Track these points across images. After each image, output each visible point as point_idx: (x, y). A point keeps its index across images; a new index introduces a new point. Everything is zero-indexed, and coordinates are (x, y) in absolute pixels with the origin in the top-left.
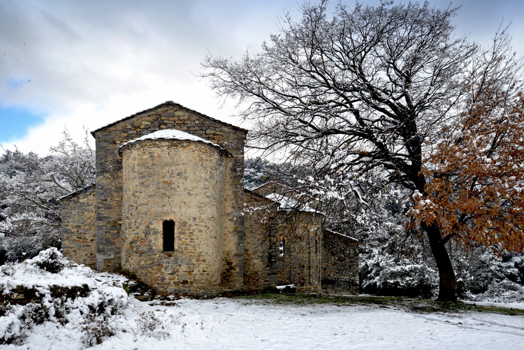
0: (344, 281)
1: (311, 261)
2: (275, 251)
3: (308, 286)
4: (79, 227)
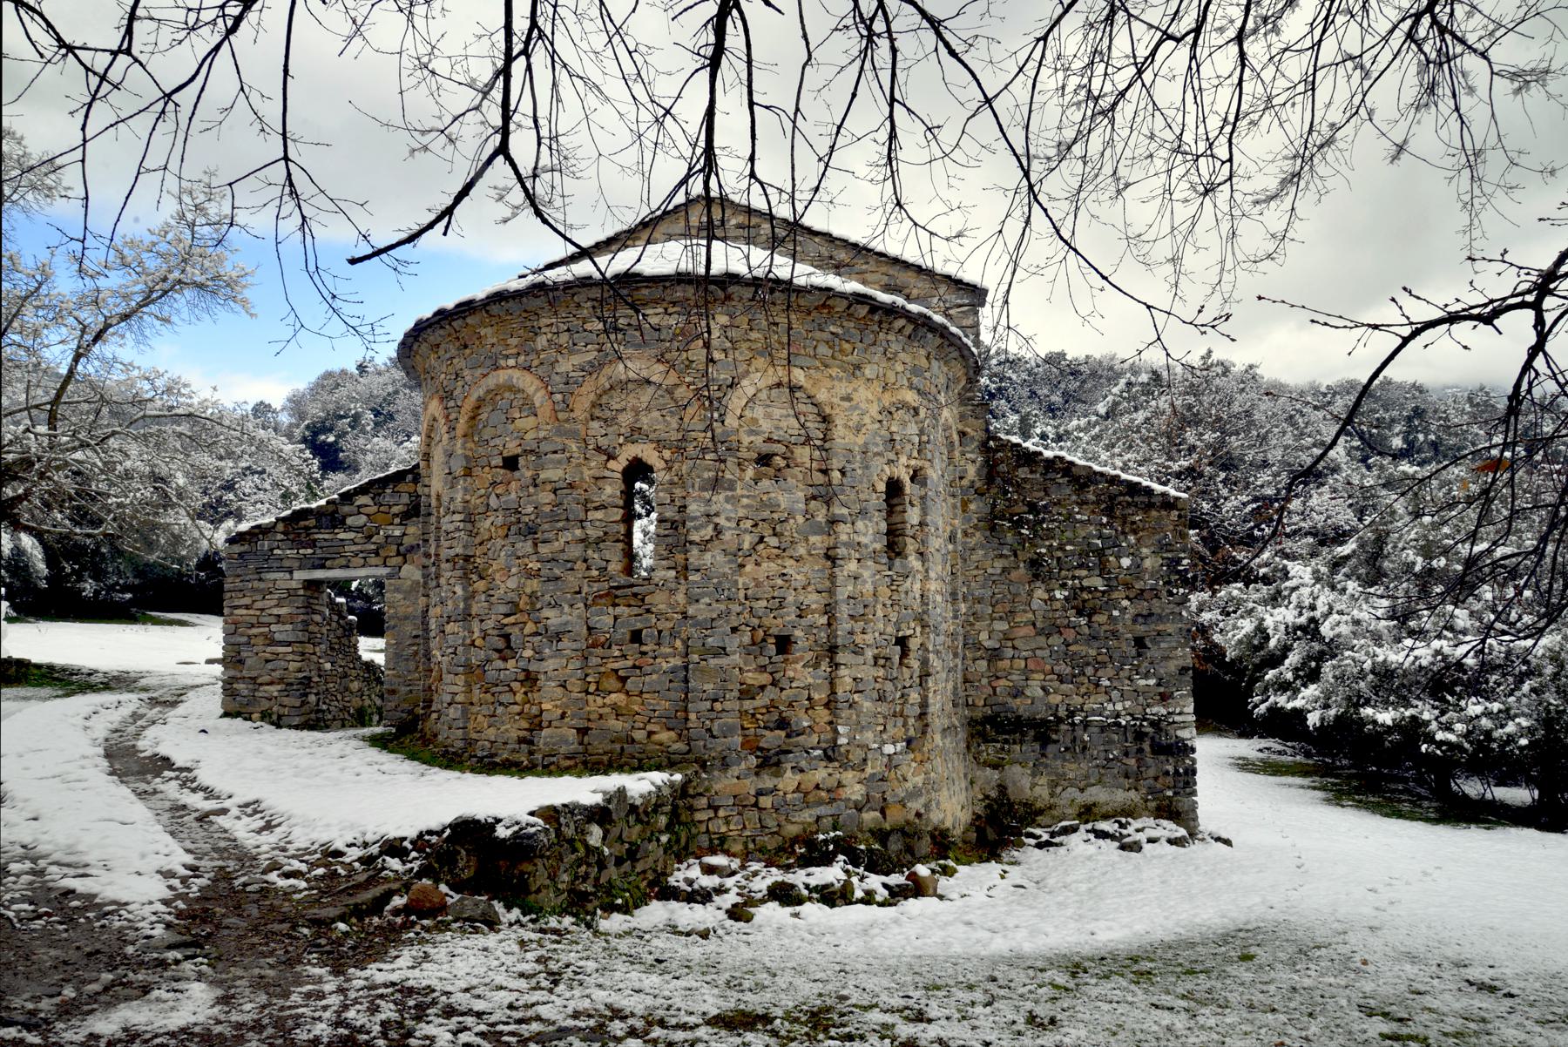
0: (1103, 728)
1: (843, 611)
3: (820, 774)
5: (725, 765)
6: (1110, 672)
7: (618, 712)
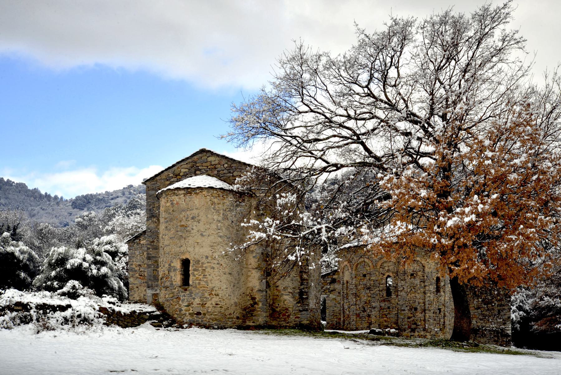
0: (490, 331)
1: (427, 303)
2: (306, 288)
4: (140, 265)
5: (405, 331)
6: (492, 318)
7: (385, 321)
